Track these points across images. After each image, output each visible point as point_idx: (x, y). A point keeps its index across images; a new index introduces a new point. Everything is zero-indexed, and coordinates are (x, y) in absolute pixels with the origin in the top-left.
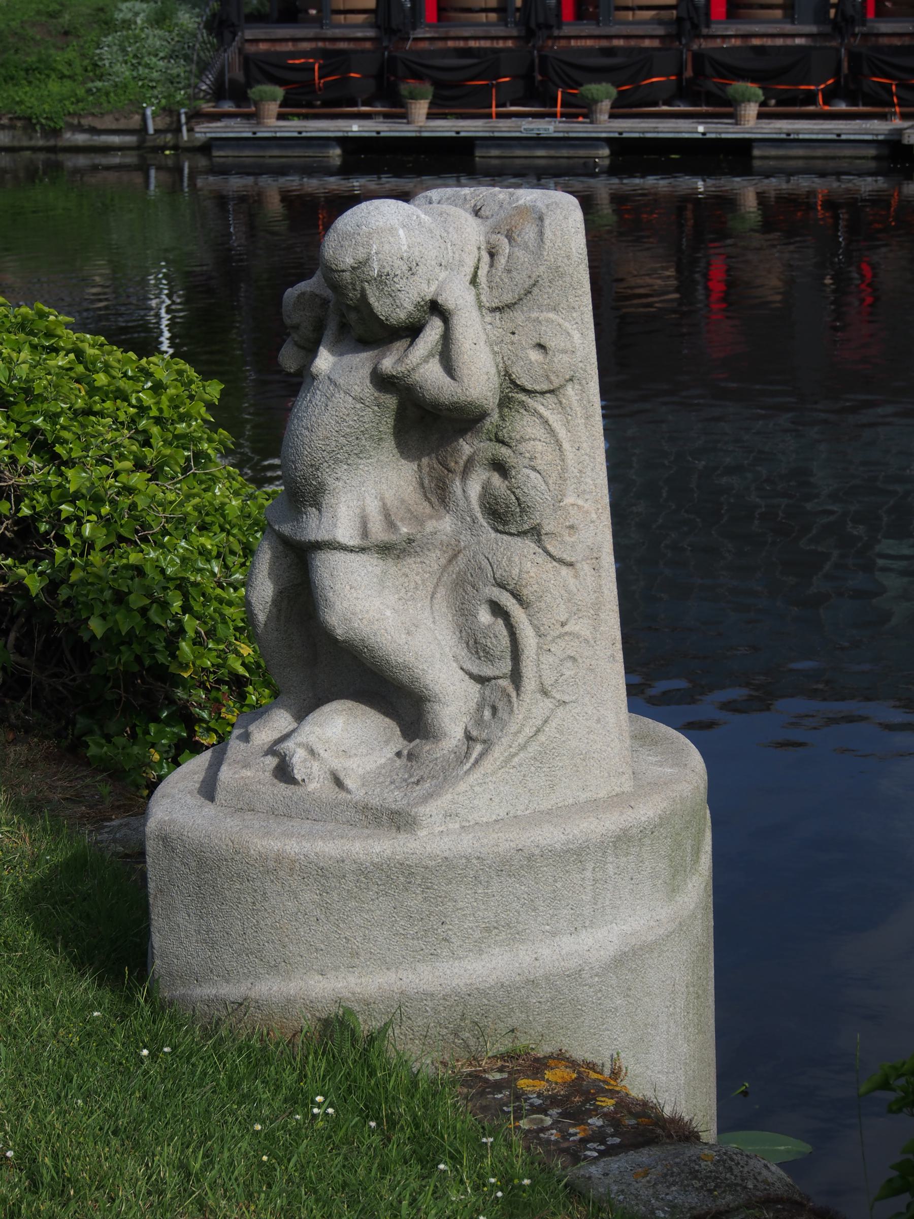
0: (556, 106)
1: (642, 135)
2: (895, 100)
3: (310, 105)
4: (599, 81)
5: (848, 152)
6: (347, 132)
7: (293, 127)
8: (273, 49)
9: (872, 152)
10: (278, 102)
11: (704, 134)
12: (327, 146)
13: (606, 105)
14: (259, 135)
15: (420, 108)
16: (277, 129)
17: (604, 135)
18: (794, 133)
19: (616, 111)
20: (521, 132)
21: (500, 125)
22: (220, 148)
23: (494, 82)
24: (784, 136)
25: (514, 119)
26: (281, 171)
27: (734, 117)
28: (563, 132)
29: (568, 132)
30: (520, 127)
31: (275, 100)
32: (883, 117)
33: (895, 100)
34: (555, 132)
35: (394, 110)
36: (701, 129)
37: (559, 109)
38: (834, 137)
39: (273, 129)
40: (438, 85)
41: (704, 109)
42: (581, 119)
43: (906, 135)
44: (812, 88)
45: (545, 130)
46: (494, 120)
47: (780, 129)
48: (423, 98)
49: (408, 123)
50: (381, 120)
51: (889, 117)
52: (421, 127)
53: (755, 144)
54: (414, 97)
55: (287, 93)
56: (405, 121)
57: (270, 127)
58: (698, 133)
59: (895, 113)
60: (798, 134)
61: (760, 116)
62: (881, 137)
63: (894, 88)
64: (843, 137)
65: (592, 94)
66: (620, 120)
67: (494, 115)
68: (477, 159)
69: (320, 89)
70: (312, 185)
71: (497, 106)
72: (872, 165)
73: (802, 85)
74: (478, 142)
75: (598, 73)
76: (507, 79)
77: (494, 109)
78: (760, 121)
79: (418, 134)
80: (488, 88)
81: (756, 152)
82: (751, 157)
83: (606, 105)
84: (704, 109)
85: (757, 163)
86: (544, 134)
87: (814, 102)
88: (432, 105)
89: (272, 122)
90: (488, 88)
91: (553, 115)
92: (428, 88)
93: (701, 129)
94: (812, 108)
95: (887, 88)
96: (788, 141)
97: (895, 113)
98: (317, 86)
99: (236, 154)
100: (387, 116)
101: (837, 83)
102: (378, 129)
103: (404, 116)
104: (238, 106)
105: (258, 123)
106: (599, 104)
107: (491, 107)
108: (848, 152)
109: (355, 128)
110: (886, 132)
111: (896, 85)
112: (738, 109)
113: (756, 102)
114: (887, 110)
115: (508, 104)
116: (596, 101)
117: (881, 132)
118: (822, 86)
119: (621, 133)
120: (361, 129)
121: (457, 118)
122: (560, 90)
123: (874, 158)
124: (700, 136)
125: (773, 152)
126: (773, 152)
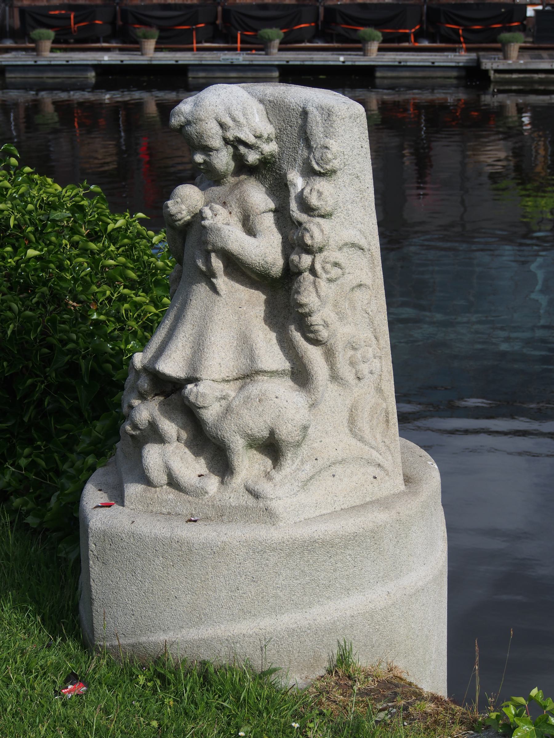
0: (236, 43)
1: (302, 63)
2: (462, 39)
3: (66, 42)
4: (271, 27)
5: (439, 74)
6: (100, 61)
7: (390, 58)
8: (33, 4)
9: (454, 74)
10: (51, 41)
11: (344, 62)
12: (86, 71)
13: (276, 43)
14: (39, 63)
15: (150, 45)
16: (51, 59)
17: (276, 63)
18: (404, 62)
19: (283, 46)
20: (220, 61)
21: (204, 56)
22: (11, 72)
23: (194, 27)
24: (397, 64)
25: (215, 52)
26: (52, 88)
27: (363, 50)
28: (249, 61)
29: (252, 61)
30: (220, 57)
31: (49, 39)
32: (454, 50)
33: (462, 39)
34: (243, 61)
35: (125, 45)
36: (342, 59)
37: (239, 45)
38: (430, 64)
39: (49, 59)
40: (161, 29)
41: (336, 45)
42: (254, 52)
43: (484, 64)
44: (407, 31)
45: (237, 59)
46: (195, 52)
47: (394, 59)
48: (152, 38)
49: (142, 55)
50: (117, 52)
51: (457, 50)
52: (151, 57)
53: (377, 69)
54: (146, 37)
55: (56, 35)
56: (140, 53)
57: (46, 57)
58: (339, 61)
59: (462, 48)
60: (406, 62)
61: (380, 50)
62: (461, 64)
63: (461, 32)
64: (436, 64)
65: (269, 36)
66: (321, 53)
67: (195, 49)
68: (190, 79)
69: (75, 31)
70: (77, 96)
71: (197, 43)
72: (454, 82)
73: (401, 29)
74: (190, 68)
75: (270, 22)
76: (202, 25)
77: (195, 45)
78: (281, 53)
79: (149, 63)
80: (191, 31)
81: (378, 74)
82: (374, 77)
83: (276, 43)
84: (336, 45)
85: (378, 81)
86: (236, 62)
87: (408, 41)
88: (157, 43)
89: (47, 54)
90: (191, 31)
91: (235, 49)
92: (155, 32)
93: (342, 59)
94: (406, 44)
95: (456, 32)
96: (400, 67)
97: (462, 48)
98: (73, 29)
99: (23, 75)
100: (121, 50)
101: (421, 28)
102: (122, 59)
103: (140, 50)
104: (16, 43)
105: (38, 55)
106: (273, 42)
107: (192, 43)
108: (439, 74)
109: (106, 58)
110: (465, 61)
111: (463, 30)
112: (366, 45)
113: (378, 41)
114: (457, 46)
115: (203, 41)
116: (270, 40)
117: (461, 61)
118: (413, 30)
119: (288, 62)
120: (110, 59)
121: (169, 51)
122: (239, 32)
123: (456, 78)
124: (341, 64)
125: (390, 74)
126: (390, 74)
